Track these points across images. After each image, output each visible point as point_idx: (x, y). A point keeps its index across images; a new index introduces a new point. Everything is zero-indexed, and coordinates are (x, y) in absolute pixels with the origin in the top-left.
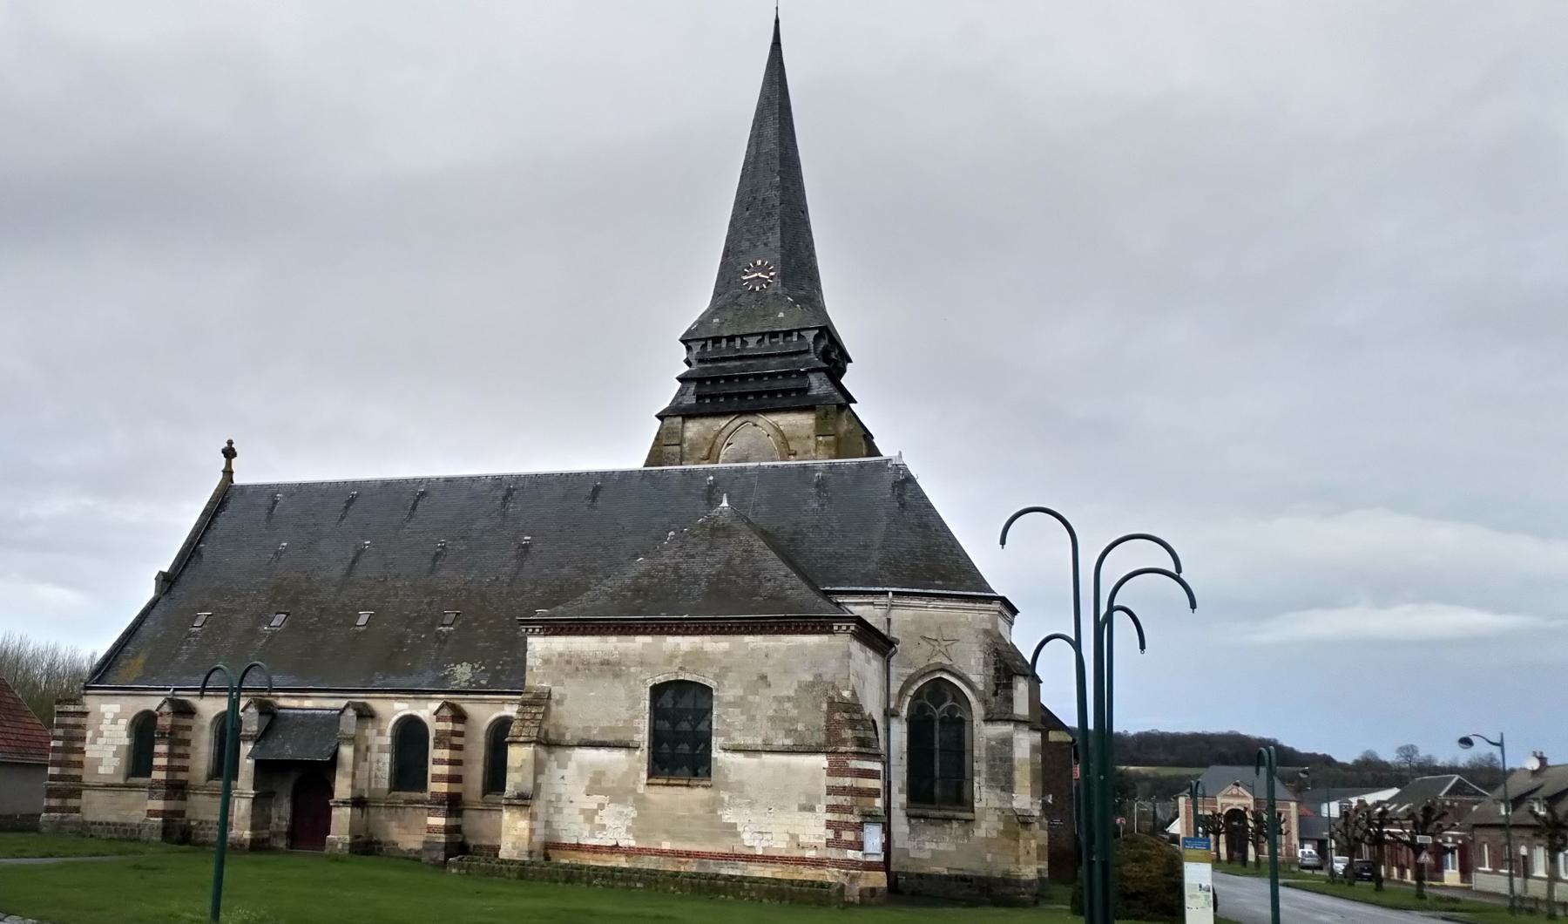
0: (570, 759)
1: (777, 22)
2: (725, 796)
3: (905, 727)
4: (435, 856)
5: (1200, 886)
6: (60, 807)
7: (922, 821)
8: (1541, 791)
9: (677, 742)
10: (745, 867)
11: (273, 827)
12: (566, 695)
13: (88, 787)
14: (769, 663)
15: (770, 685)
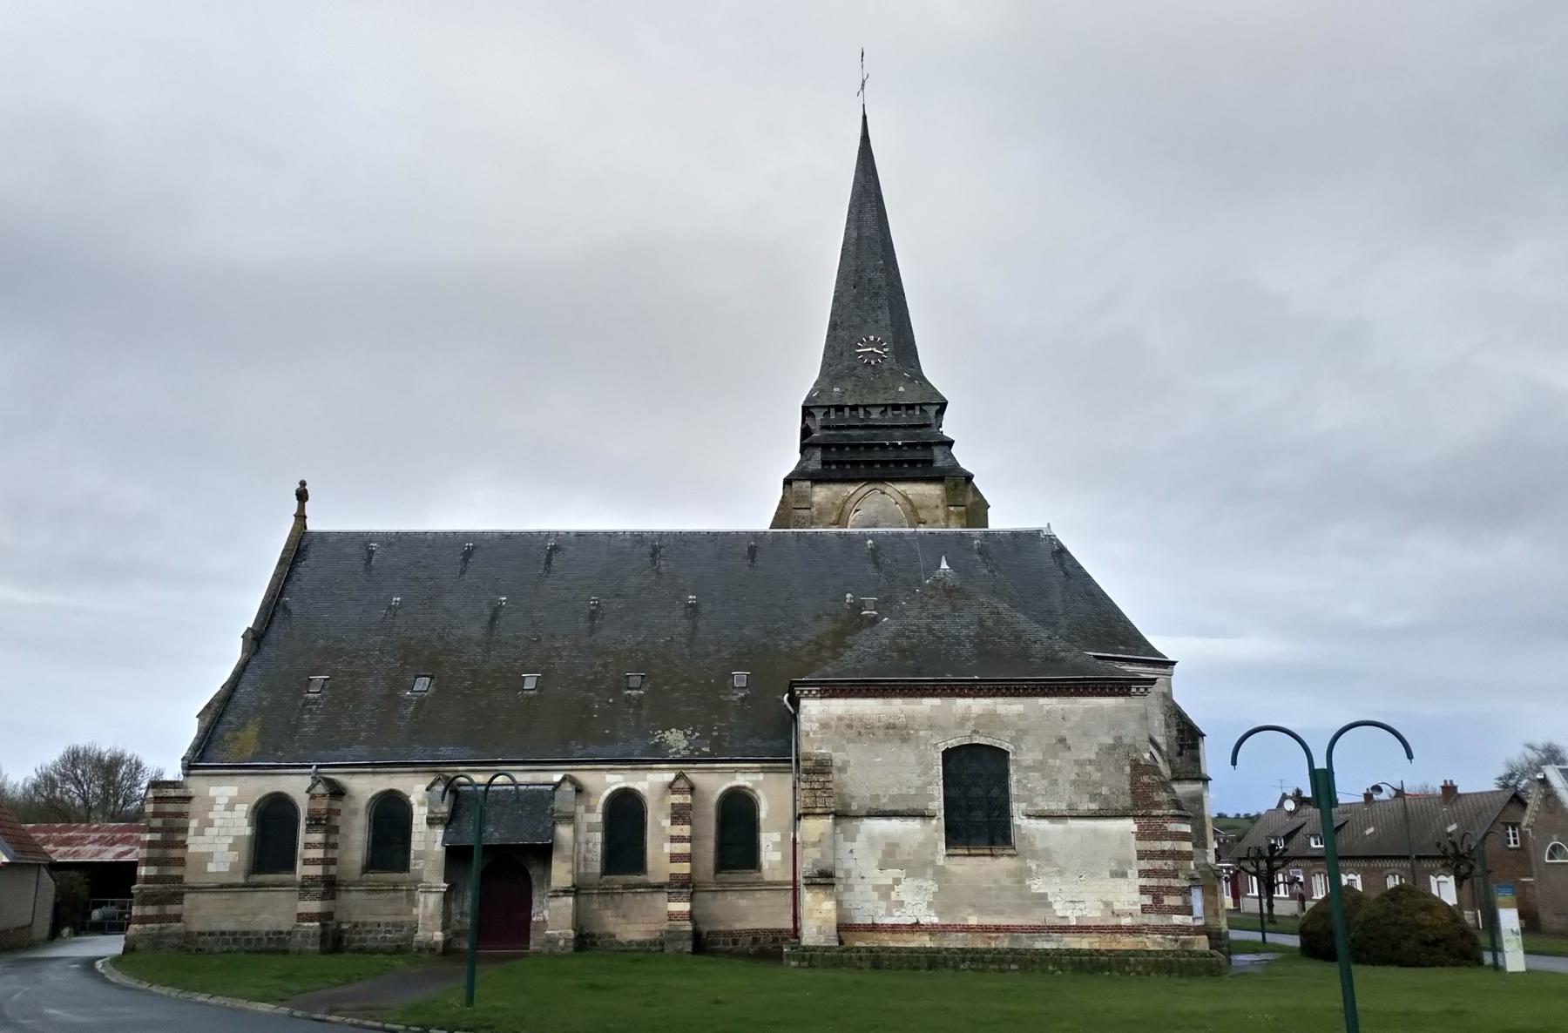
1: (865, 117)
2: (1033, 865)
4: (680, 947)
5: (1512, 931)
8: (1304, 828)
9: (970, 809)
10: (1060, 939)
12: (849, 762)
13: (194, 889)
15: (1069, 748)
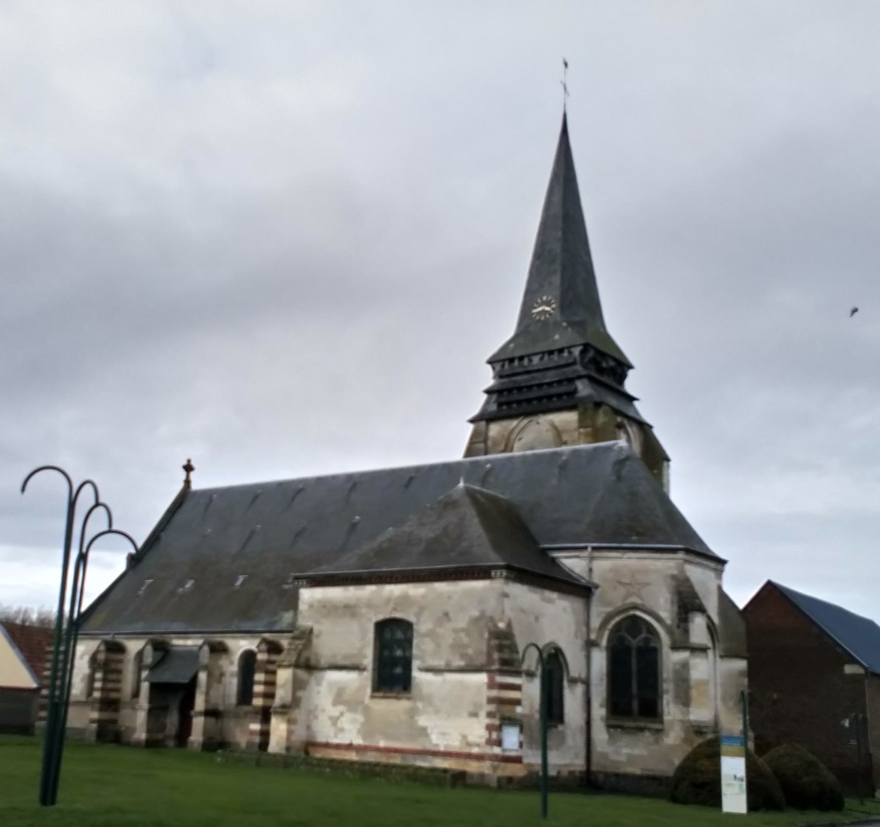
1: (565, 105)
2: (420, 705)
5: (735, 777)
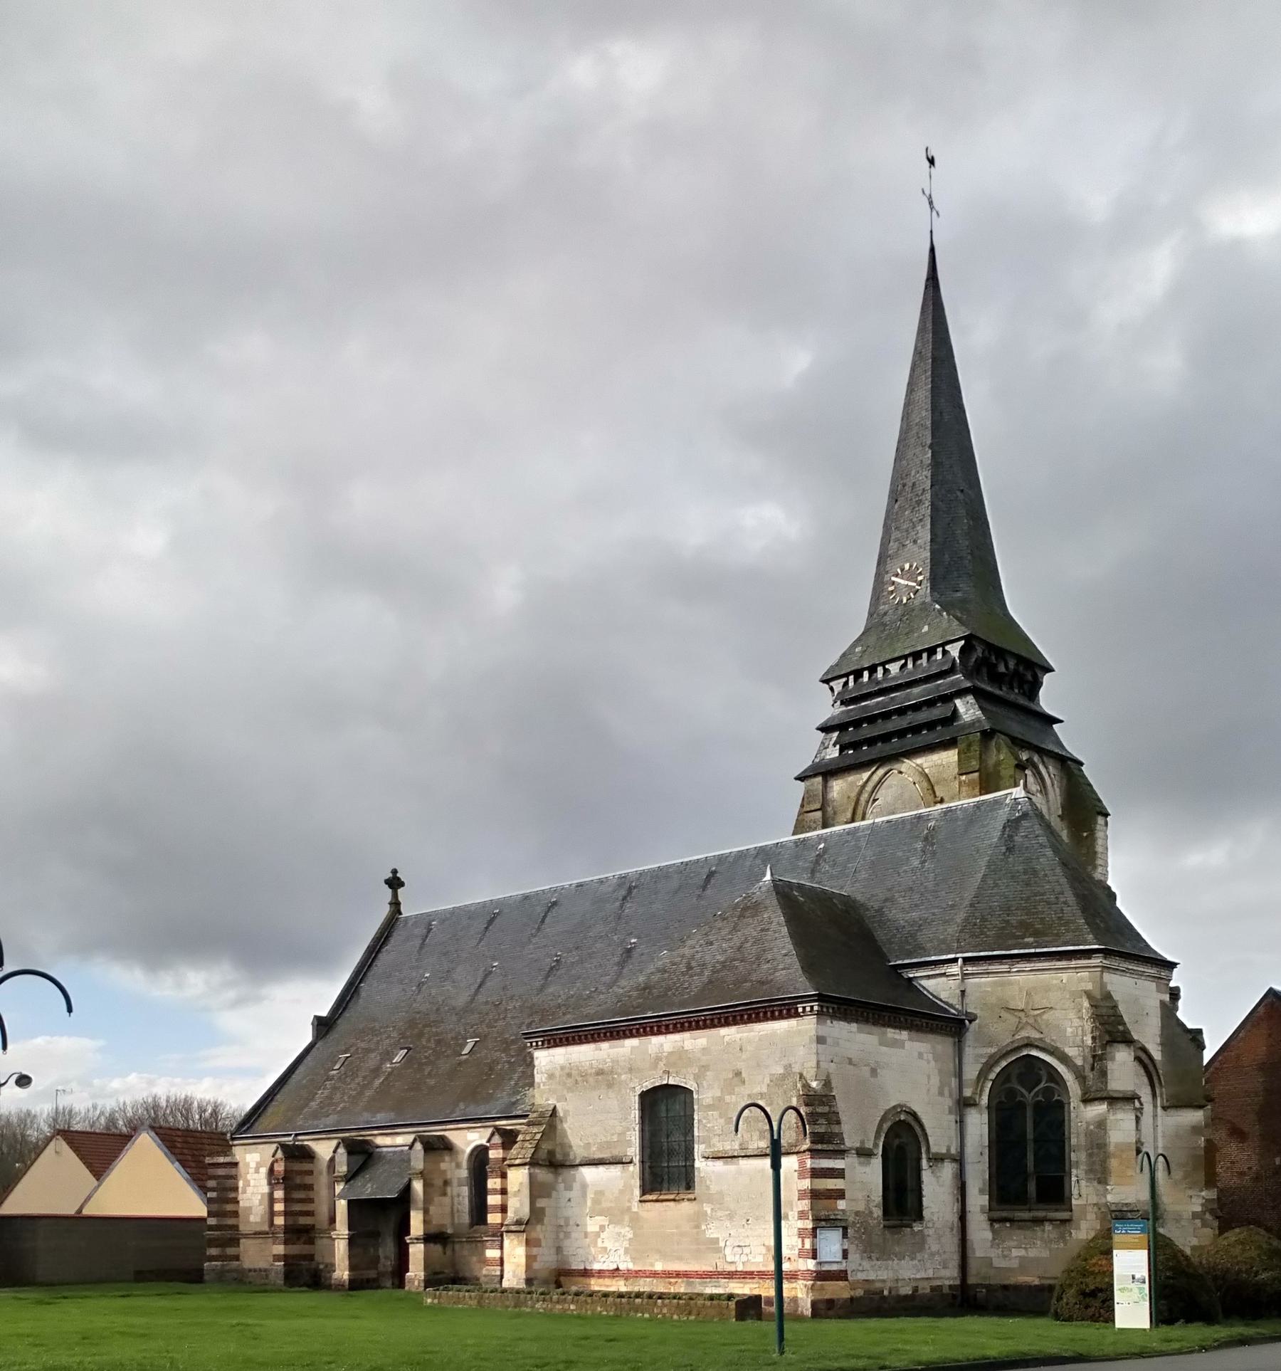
0: (574, 1181)
1: (932, 250)
3: (985, 1117)
5: (1133, 1277)
6: (220, 1256)
7: (1008, 1225)
11: (381, 1268)
13: (246, 1236)
14: (744, 1057)
15: (744, 1082)
